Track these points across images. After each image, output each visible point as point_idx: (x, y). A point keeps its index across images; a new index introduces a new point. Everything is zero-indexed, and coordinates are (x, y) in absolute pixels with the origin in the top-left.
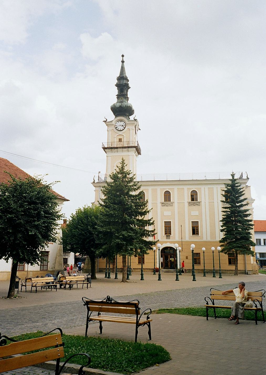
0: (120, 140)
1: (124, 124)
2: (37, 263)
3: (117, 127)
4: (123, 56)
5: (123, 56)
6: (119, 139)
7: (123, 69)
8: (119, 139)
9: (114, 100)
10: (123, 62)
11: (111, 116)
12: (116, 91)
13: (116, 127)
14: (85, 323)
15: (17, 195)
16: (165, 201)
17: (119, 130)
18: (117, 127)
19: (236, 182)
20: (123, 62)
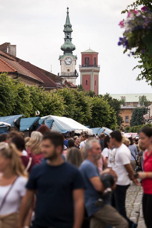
0: (68, 70)
1: (71, 61)
2: (144, 70)
3: (67, 59)
4: (68, 8)
5: (68, 8)
6: (68, 70)
7: (68, 18)
8: (68, 70)
9: (62, 42)
10: (68, 13)
11: (62, 53)
12: (63, 35)
13: (67, 59)
14: (139, 205)
15: (95, 117)
17: (68, 64)
18: (67, 59)
19: (143, 69)
20: (68, 13)
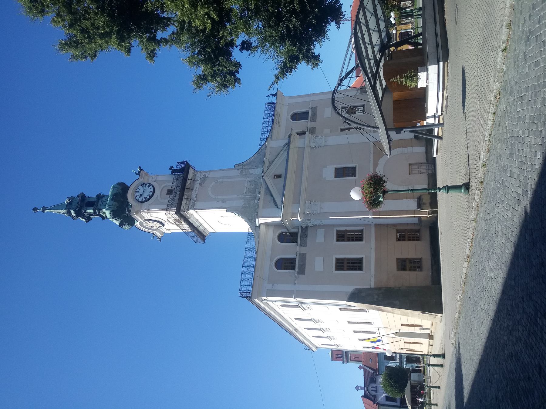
16: (294, 269)
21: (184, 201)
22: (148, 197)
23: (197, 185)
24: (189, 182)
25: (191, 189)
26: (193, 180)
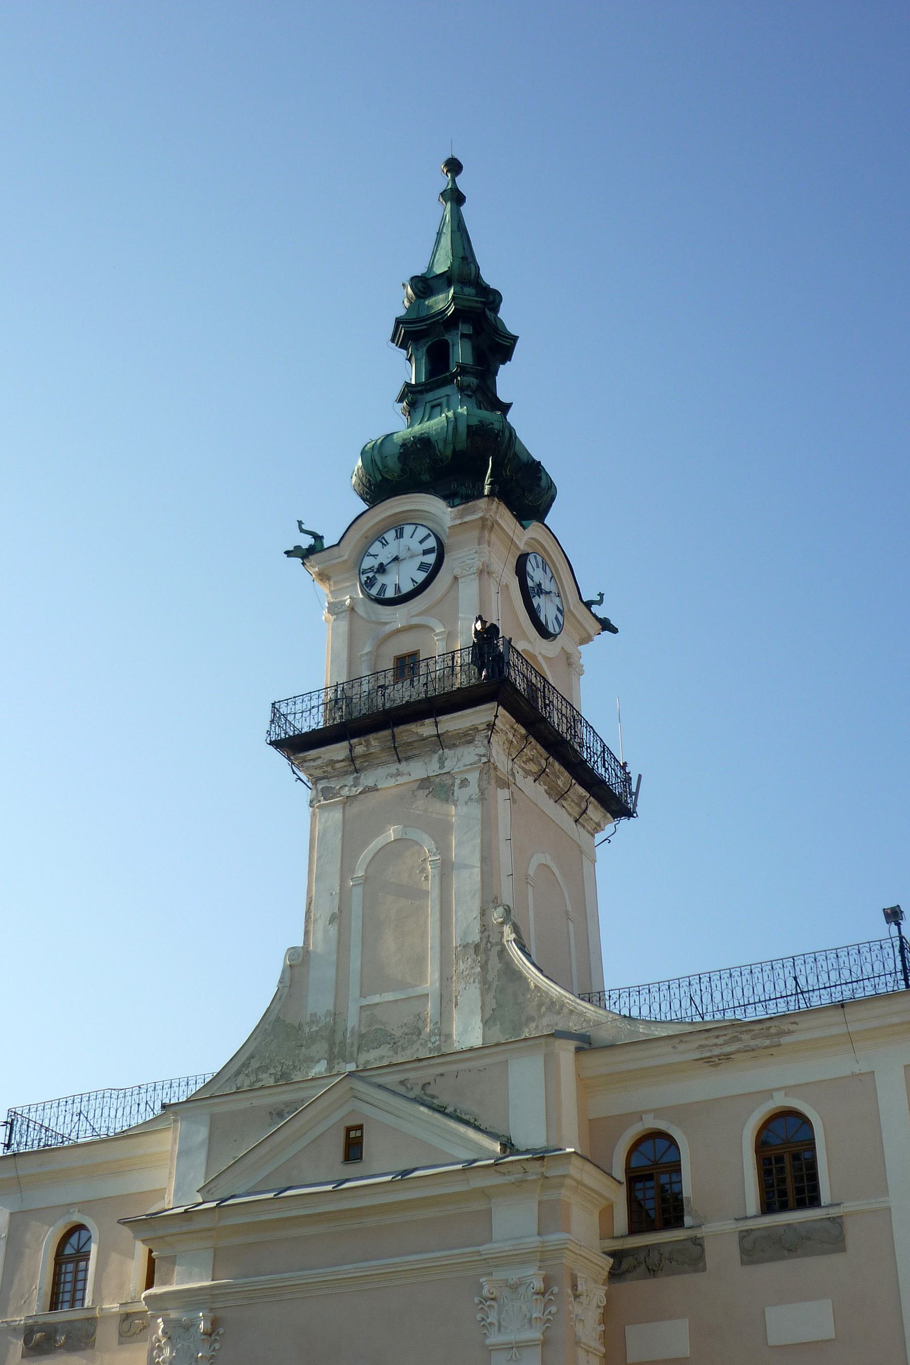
5: (454, 166)
21: (338, 751)
22: (390, 593)
23: (417, 770)
24: (426, 729)
25: (400, 753)
26: (441, 742)
